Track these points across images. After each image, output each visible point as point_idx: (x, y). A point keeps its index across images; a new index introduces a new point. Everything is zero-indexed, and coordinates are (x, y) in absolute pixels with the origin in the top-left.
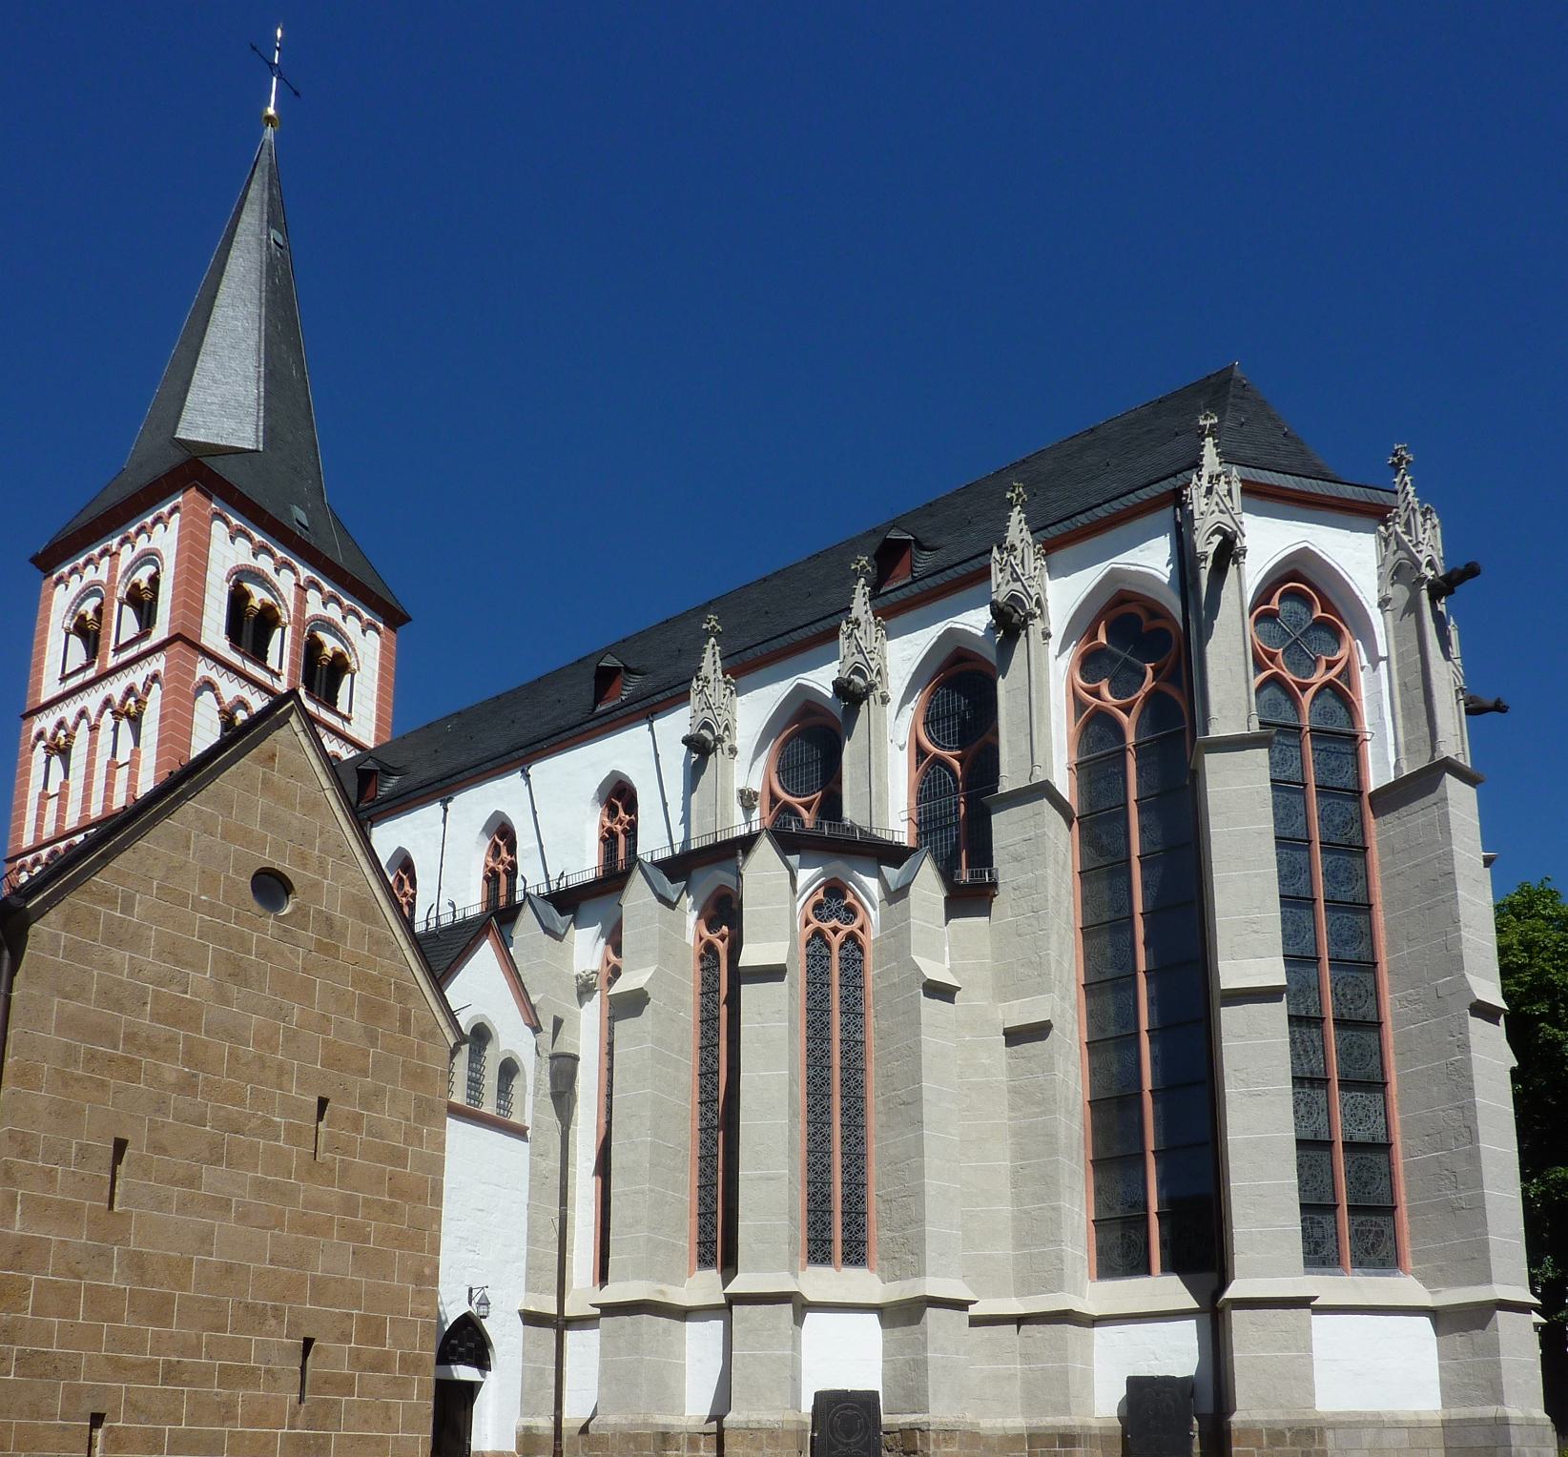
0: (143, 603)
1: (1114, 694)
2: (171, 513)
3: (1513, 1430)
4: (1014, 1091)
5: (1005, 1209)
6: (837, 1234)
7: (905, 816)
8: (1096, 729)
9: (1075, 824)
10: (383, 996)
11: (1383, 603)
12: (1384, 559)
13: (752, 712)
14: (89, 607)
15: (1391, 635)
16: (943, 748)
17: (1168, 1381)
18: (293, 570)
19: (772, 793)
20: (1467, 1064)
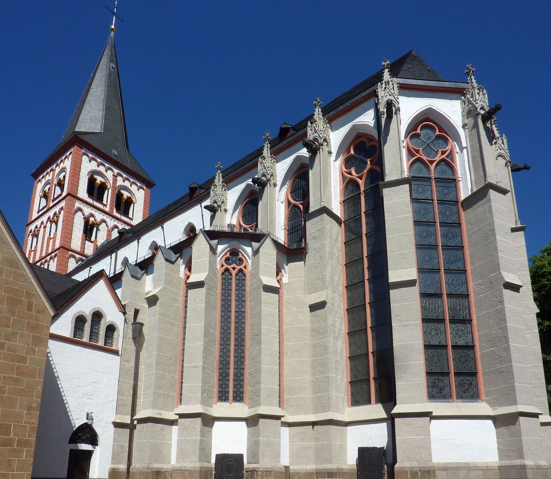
0: (61, 184)
1: (357, 173)
2: (70, 155)
3: (528, 471)
4: (313, 330)
5: (308, 378)
6: (231, 389)
7: (283, 228)
8: (350, 185)
9: (343, 224)
10: (19, 296)
11: (464, 126)
12: (464, 109)
13: (233, 195)
14: (47, 189)
15: (468, 138)
16: (297, 201)
17: (374, 449)
18: (112, 170)
19: (240, 225)
20: (503, 309)
